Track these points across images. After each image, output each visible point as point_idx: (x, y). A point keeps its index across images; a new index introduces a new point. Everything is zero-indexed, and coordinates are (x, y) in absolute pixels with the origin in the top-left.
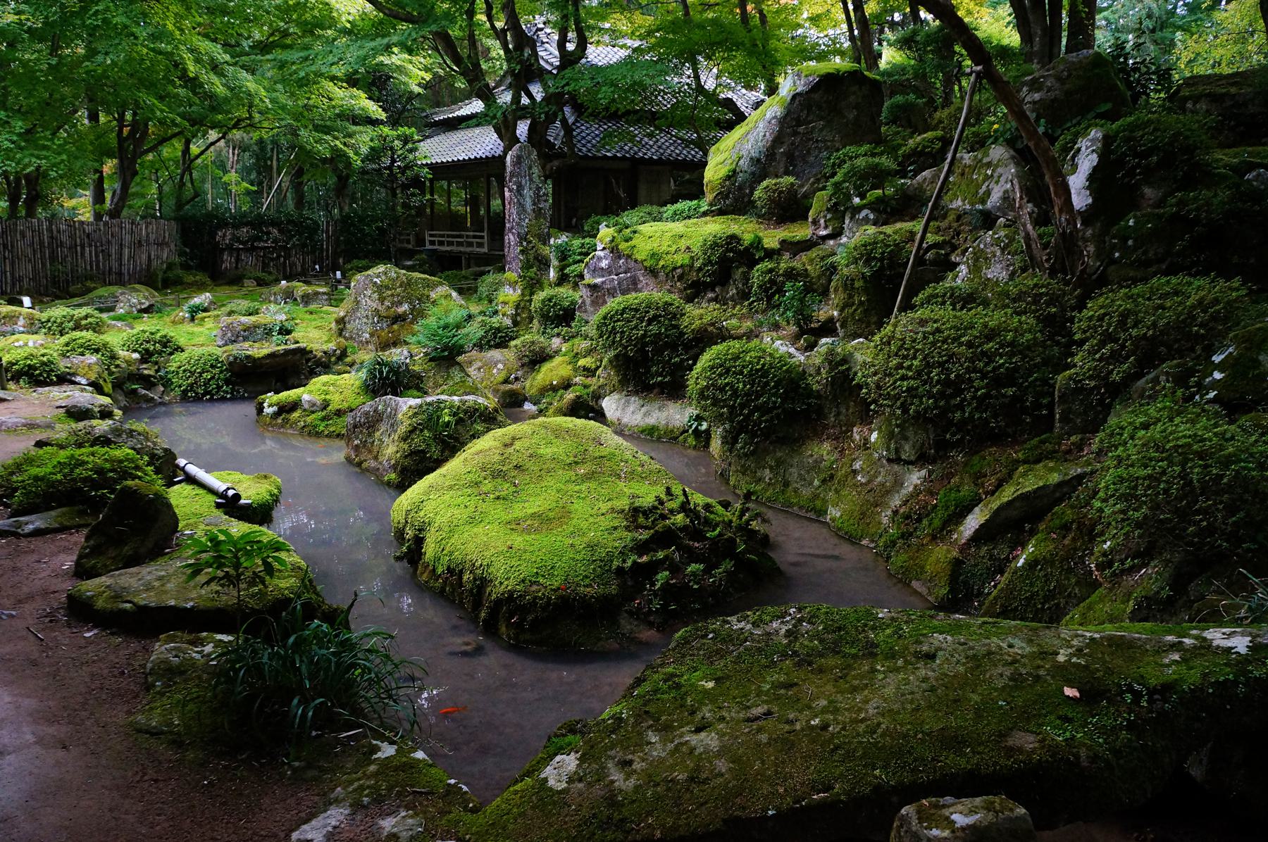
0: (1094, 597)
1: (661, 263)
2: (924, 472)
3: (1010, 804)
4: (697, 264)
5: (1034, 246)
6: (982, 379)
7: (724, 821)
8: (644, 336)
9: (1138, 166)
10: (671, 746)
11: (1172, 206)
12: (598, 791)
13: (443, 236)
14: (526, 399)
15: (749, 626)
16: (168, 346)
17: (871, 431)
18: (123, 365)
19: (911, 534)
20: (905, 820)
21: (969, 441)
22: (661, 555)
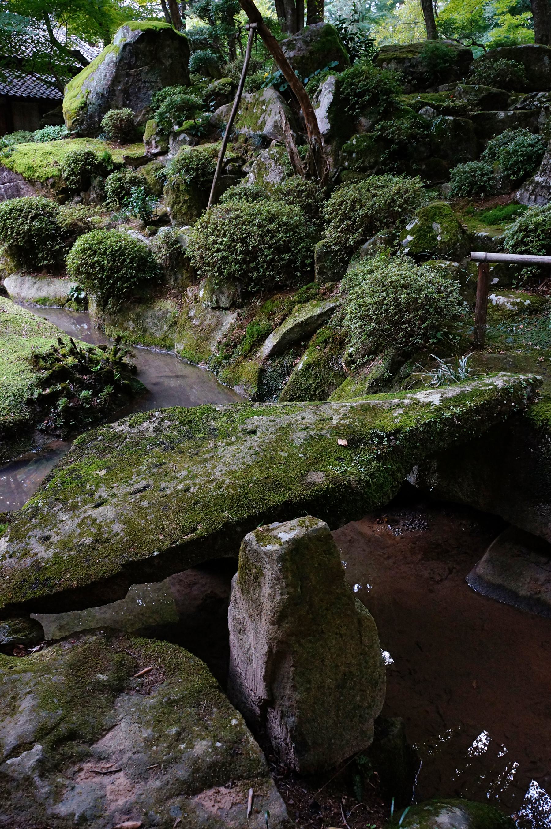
0: (344, 383)
1: (37, 174)
2: (236, 315)
3: (316, 520)
4: (65, 175)
5: (296, 157)
6: (269, 249)
7: (122, 565)
8: (29, 230)
9: (357, 103)
10: (78, 521)
11: (378, 130)
12: (28, 562)
15: (127, 428)
17: (199, 289)
19: (230, 356)
20: (247, 544)
21: (263, 291)
22: (59, 387)
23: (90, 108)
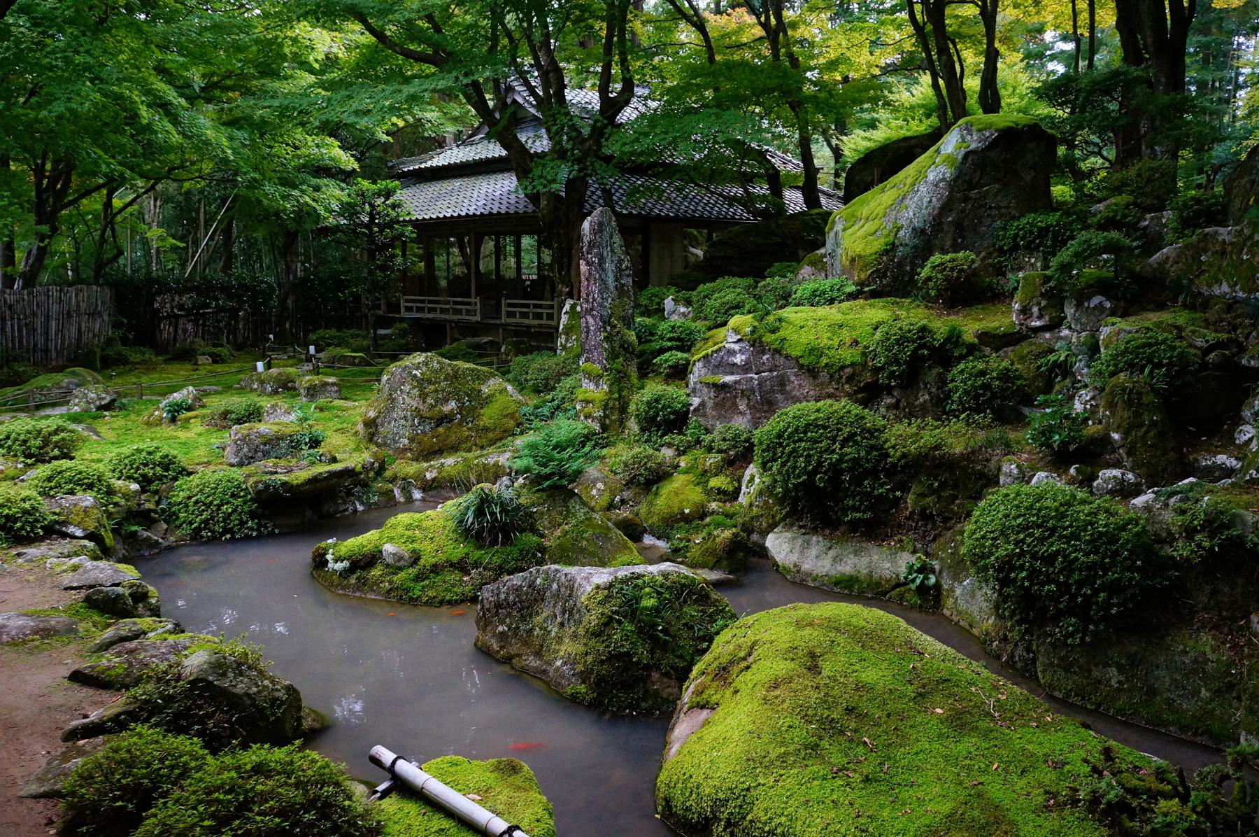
8: (840, 461)
13: (423, 302)
14: (645, 531)
16: (171, 469)
18: (123, 502)
23: (900, 252)
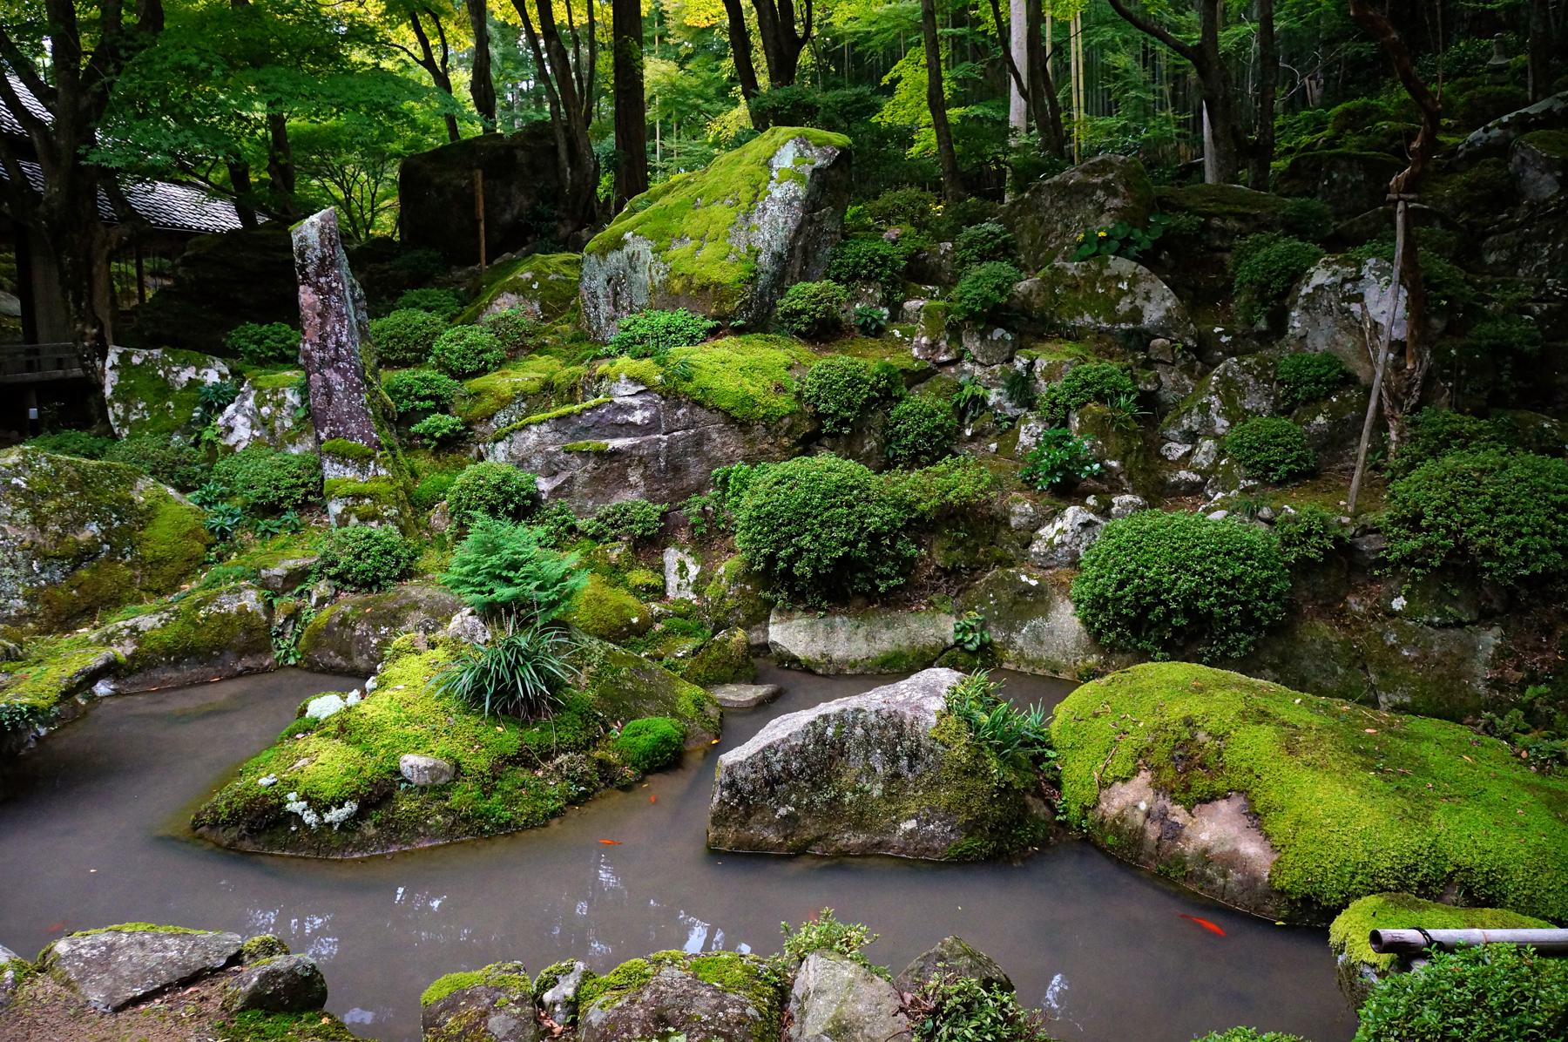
23: (763, 279)
